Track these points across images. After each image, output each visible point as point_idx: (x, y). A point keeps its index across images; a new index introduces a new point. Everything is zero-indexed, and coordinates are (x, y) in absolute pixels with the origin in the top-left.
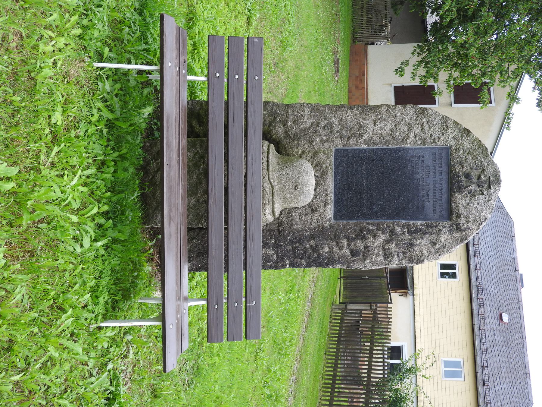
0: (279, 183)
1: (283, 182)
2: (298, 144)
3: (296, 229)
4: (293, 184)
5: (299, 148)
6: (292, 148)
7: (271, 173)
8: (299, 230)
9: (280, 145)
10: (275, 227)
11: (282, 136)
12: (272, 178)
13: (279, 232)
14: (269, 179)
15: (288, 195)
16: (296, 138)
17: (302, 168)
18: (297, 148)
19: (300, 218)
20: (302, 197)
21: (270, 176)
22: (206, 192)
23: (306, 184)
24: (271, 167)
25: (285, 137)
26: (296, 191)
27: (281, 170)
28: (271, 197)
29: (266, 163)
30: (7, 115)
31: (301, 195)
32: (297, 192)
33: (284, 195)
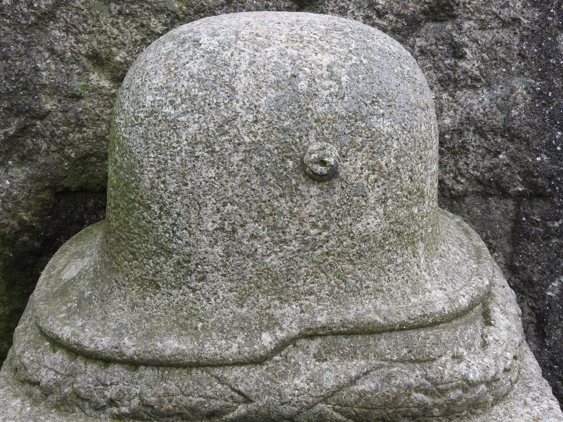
0: (280, 285)
1: (273, 261)
2: (55, 90)
3: (531, 111)
4: (292, 192)
5: (77, 84)
6: (80, 125)
7: (210, 350)
8: (539, 95)
9: (71, 183)
10: (500, 210)
11: (20, 173)
12: (252, 335)
13: (536, 193)
14: (257, 361)
15: (372, 222)
16: (24, 100)
17: (174, 125)
18: (77, 97)
19: (474, 83)
20: (384, 126)
21: (234, 348)
22: (258, 9)
23: (293, 98)
24: (171, 345)
25: (23, 160)
26: (346, 168)
27: (188, 270)
28: (383, 343)
29: (149, 373)
30: (146, 374)
31: (374, 136)
32: (354, 168)
33: (366, 251)
